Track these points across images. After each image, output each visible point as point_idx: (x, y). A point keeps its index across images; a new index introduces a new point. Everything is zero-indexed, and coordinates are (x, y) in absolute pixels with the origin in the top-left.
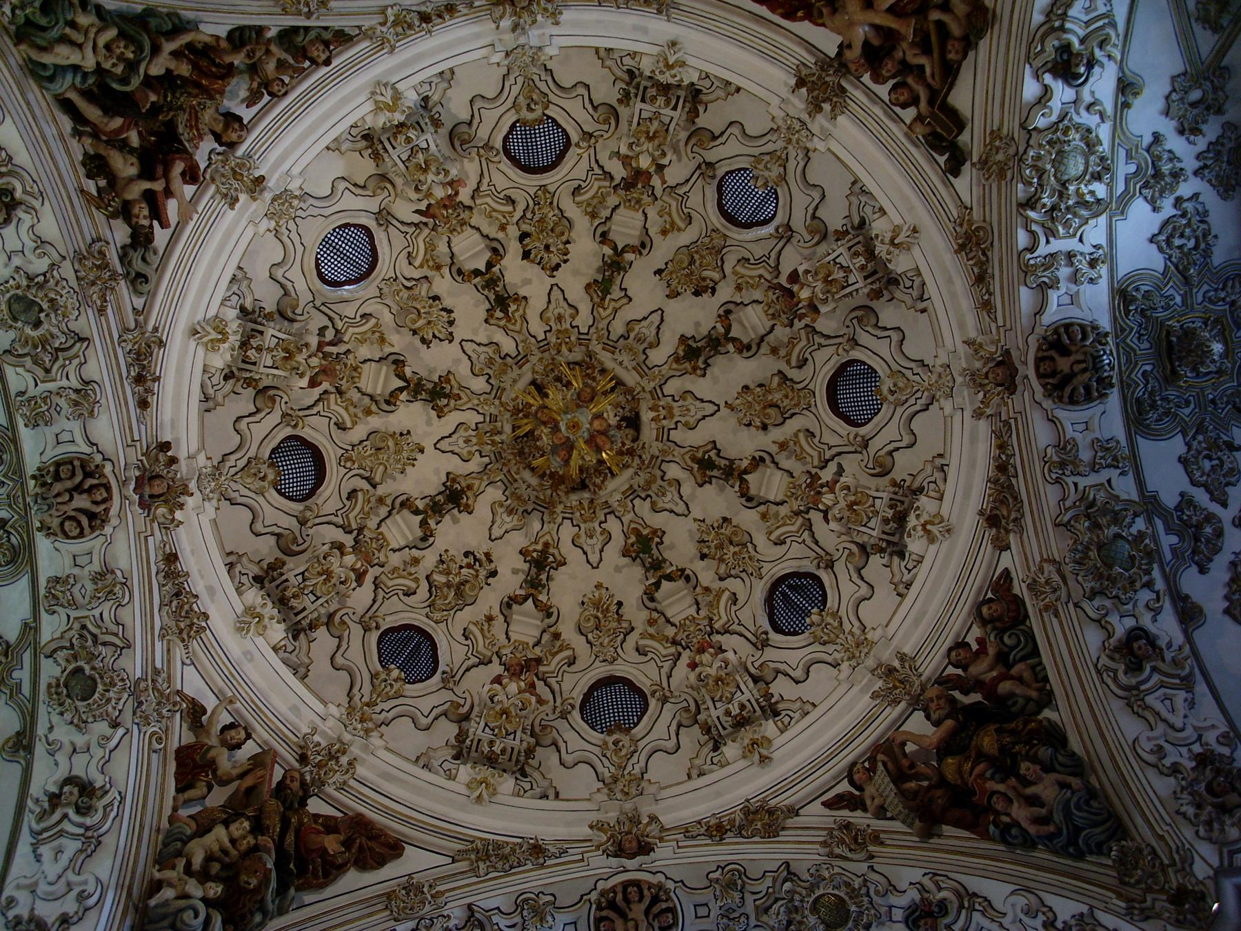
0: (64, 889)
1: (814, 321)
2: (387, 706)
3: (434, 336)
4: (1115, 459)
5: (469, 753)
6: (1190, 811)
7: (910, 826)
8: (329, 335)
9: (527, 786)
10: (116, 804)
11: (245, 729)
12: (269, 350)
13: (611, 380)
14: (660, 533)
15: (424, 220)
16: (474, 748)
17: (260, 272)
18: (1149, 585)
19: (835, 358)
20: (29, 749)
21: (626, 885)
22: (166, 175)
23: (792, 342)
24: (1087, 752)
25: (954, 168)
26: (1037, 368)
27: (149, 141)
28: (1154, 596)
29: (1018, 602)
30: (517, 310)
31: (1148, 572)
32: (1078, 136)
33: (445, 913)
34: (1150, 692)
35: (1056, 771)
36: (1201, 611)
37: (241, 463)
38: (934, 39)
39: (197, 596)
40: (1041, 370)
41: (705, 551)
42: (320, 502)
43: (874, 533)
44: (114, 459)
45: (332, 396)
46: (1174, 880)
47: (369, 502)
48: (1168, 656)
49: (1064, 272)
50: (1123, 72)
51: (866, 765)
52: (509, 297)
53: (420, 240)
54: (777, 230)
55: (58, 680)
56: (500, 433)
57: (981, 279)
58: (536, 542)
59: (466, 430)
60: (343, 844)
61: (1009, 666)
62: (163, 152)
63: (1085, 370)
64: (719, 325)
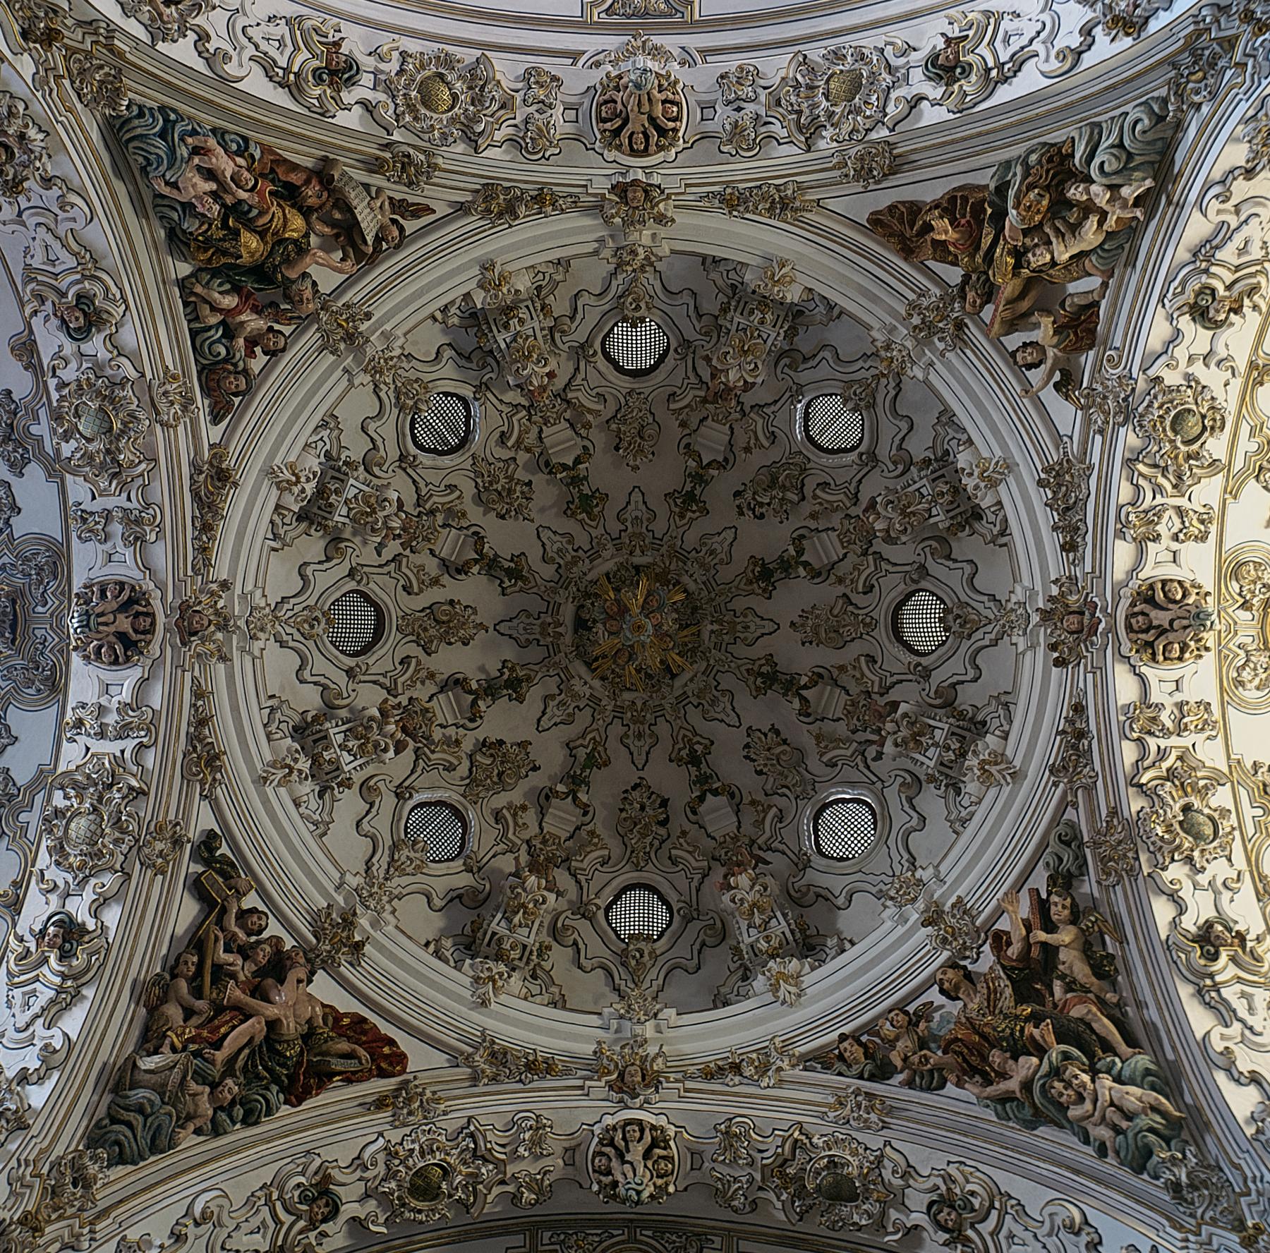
0: (1244, 207)
1: (386, 701)
2: (863, 374)
3: (766, 735)
4: (84, 520)
5: (787, 315)
6: (32, 132)
7: (344, 174)
8: (871, 751)
9: (732, 275)
10: (1169, 295)
11: (1016, 363)
12: (936, 745)
13: (596, 669)
14: (568, 512)
15: (761, 853)
16: (781, 320)
17: (938, 825)
18: (62, 385)
19: (371, 662)
20: (1252, 365)
21: (645, 153)
22: (1028, 945)
23: (413, 682)
24: (149, 225)
25: (210, 840)
26: (153, 624)
27: (1043, 984)
28: (58, 372)
29: (207, 391)
30: (680, 750)
31: (62, 398)
32: (72, 859)
33: (835, 144)
34: (71, 270)
35: (182, 204)
36: (12, 350)
37: (979, 635)
38: (208, 979)
39: (1046, 505)
40: (149, 620)
41: (526, 489)
42: (902, 586)
43: (352, 481)
44: (1117, 655)
45: (876, 690)
46: (57, 56)
47: (852, 580)
48: (48, 306)
49: (111, 719)
50: (13, 920)
51: (385, 246)
52: (686, 764)
53: (768, 834)
54: (411, 796)
55: (1211, 434)
56: (712, 632)
57: (202, 722)
58: (692, 519)
59: (746, 639)
60: (931, 228)
61: (223, 323)
62: (1032, 972)
63: (102, 614)
64: (483, 708)
